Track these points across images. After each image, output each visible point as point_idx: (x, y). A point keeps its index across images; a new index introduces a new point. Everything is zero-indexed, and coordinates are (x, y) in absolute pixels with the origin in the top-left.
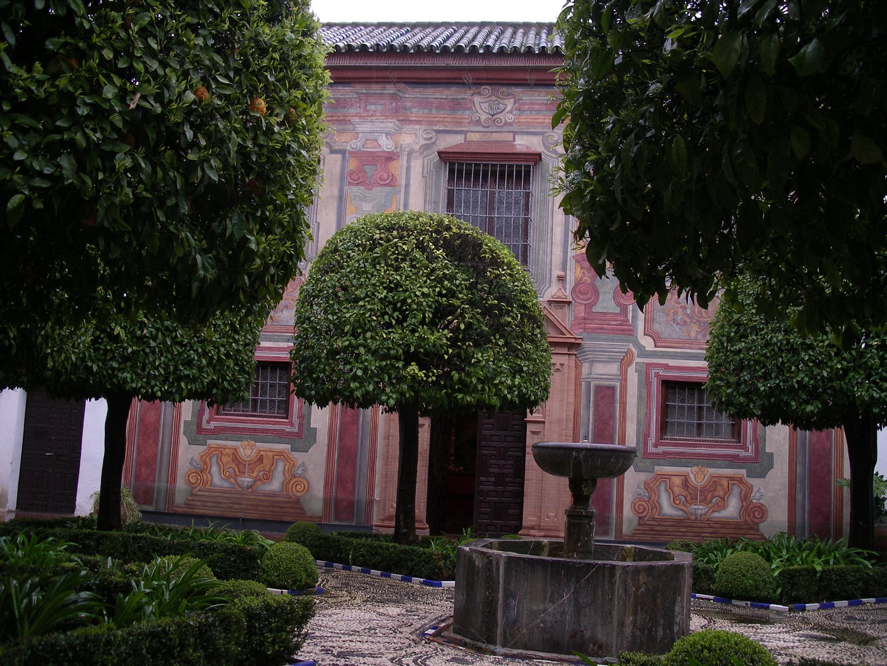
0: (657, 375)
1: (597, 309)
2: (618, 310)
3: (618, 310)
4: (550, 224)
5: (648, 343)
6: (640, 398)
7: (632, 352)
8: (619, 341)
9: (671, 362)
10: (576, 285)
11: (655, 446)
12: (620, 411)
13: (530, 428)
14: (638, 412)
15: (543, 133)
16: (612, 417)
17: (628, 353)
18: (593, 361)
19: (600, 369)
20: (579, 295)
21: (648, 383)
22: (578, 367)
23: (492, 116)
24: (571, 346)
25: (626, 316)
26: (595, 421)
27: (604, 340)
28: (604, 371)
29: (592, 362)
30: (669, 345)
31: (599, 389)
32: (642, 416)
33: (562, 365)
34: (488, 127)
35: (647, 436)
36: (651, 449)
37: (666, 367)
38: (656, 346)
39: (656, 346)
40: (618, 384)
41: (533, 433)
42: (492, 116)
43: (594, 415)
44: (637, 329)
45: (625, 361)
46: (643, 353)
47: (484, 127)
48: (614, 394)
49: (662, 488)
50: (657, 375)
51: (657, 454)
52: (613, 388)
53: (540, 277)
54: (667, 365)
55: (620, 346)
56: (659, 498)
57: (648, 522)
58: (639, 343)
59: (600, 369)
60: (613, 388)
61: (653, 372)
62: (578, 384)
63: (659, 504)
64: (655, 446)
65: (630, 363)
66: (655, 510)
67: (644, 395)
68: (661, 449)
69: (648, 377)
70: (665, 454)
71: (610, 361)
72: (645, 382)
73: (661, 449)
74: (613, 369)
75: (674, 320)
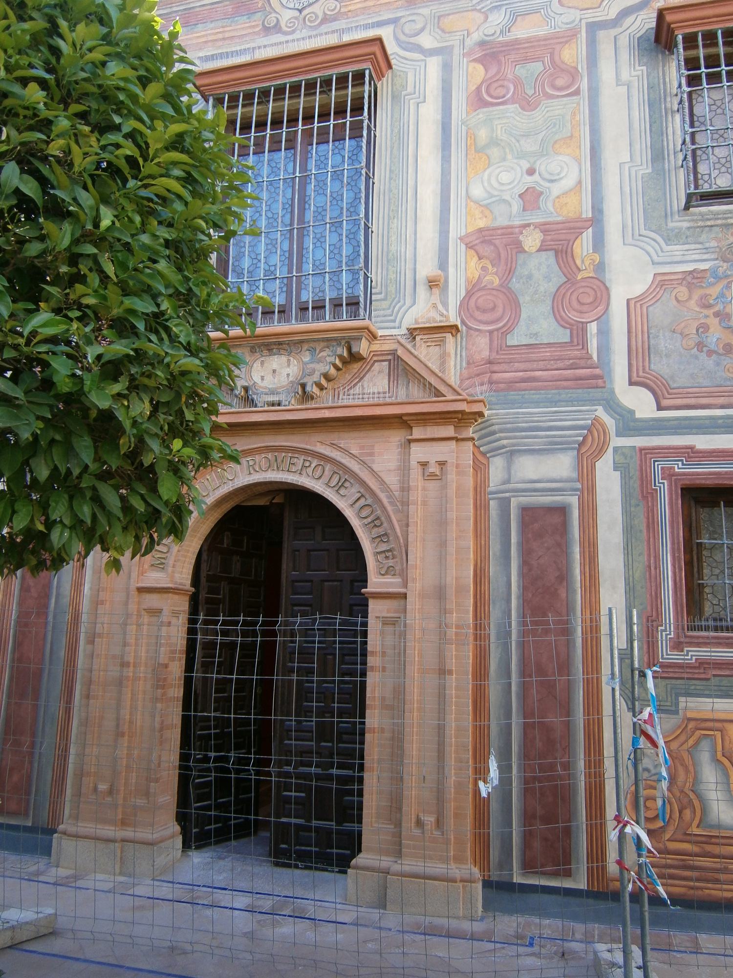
0: (669, 474)
1: (516, 339)
2: (564, 336)
3: (564, 336)
4: (411, 183)
5: (641, 404)
6: (629, 530)
7: (603, 426)
8: (570, 402)
9: (702, 442)
10: (469, 294)
11: (678, 646)
12: (583, 565)
13: (375, 608)
14: (627, 565)
15: (395, 21)
16: (564, 577)
17: (595, 428)
18: (512, 453)
19: (529, 468)
20: (477, 314)
21: (648, 495)
22: (480, 467)
23: (300, 11)
24: (459, 419)
25: (584, 345)
26: (524, 588)
27: (537, 404)
28: (545, 471)
29: (512, 454)
30: (692, 401)
31: (529, 514)
32: (639, 571)
33: (442, 464)
34: (293, 32)
35: (652, 622)
36: (666, 654)
37: (691, 454)
38: (660, 408)
39: (660, 408)
40: (574, 501)
41: (386, 622)
42: (300, 11)
43: (522, 575)
44: (610, 372)
45: (588, 447)
46: (630, 424)
47: (286, 33)
48: (563, 528)
49: (705, 756)
50: (669, 474)
51: (680, 666)
52: (562, 511)
53: (392, 288)
54: (692, 448)
55: (575, 415)
56: (696, 780)
57: (672, 846)
58: (619, 405)
59: (529, 468)
60: (562, 511)
61: (659, 466)
62: (481, 507)
63: (699, 797)
64: (678, 646)
65: (600, 451)
66: (687, 813)
67: (640, 522)
68: (692, 654)
69: (645, 480)
70: (702, 664)
71: (552, 448)
72: (638, 492)
73: (692, 654)
74: (562, 466)
75: (700, 346)
